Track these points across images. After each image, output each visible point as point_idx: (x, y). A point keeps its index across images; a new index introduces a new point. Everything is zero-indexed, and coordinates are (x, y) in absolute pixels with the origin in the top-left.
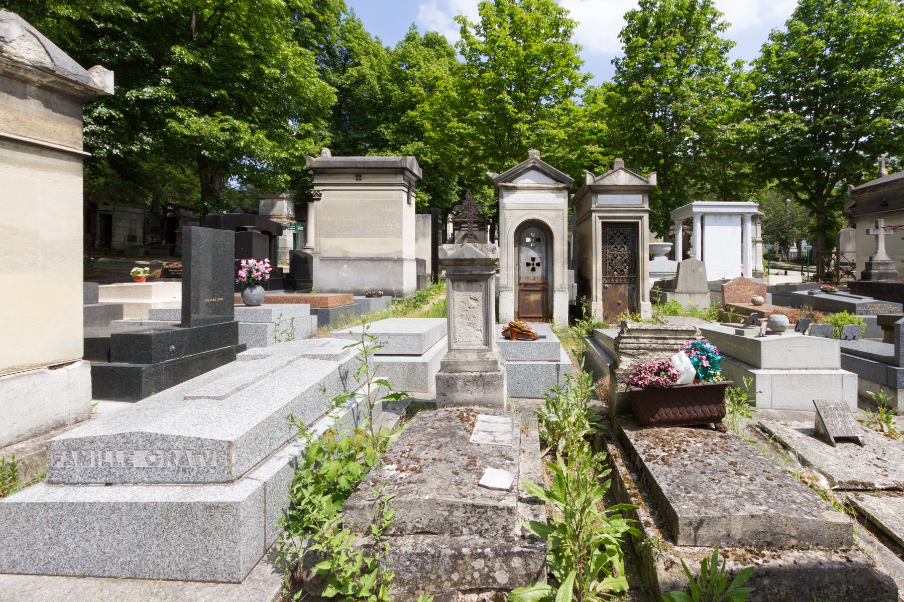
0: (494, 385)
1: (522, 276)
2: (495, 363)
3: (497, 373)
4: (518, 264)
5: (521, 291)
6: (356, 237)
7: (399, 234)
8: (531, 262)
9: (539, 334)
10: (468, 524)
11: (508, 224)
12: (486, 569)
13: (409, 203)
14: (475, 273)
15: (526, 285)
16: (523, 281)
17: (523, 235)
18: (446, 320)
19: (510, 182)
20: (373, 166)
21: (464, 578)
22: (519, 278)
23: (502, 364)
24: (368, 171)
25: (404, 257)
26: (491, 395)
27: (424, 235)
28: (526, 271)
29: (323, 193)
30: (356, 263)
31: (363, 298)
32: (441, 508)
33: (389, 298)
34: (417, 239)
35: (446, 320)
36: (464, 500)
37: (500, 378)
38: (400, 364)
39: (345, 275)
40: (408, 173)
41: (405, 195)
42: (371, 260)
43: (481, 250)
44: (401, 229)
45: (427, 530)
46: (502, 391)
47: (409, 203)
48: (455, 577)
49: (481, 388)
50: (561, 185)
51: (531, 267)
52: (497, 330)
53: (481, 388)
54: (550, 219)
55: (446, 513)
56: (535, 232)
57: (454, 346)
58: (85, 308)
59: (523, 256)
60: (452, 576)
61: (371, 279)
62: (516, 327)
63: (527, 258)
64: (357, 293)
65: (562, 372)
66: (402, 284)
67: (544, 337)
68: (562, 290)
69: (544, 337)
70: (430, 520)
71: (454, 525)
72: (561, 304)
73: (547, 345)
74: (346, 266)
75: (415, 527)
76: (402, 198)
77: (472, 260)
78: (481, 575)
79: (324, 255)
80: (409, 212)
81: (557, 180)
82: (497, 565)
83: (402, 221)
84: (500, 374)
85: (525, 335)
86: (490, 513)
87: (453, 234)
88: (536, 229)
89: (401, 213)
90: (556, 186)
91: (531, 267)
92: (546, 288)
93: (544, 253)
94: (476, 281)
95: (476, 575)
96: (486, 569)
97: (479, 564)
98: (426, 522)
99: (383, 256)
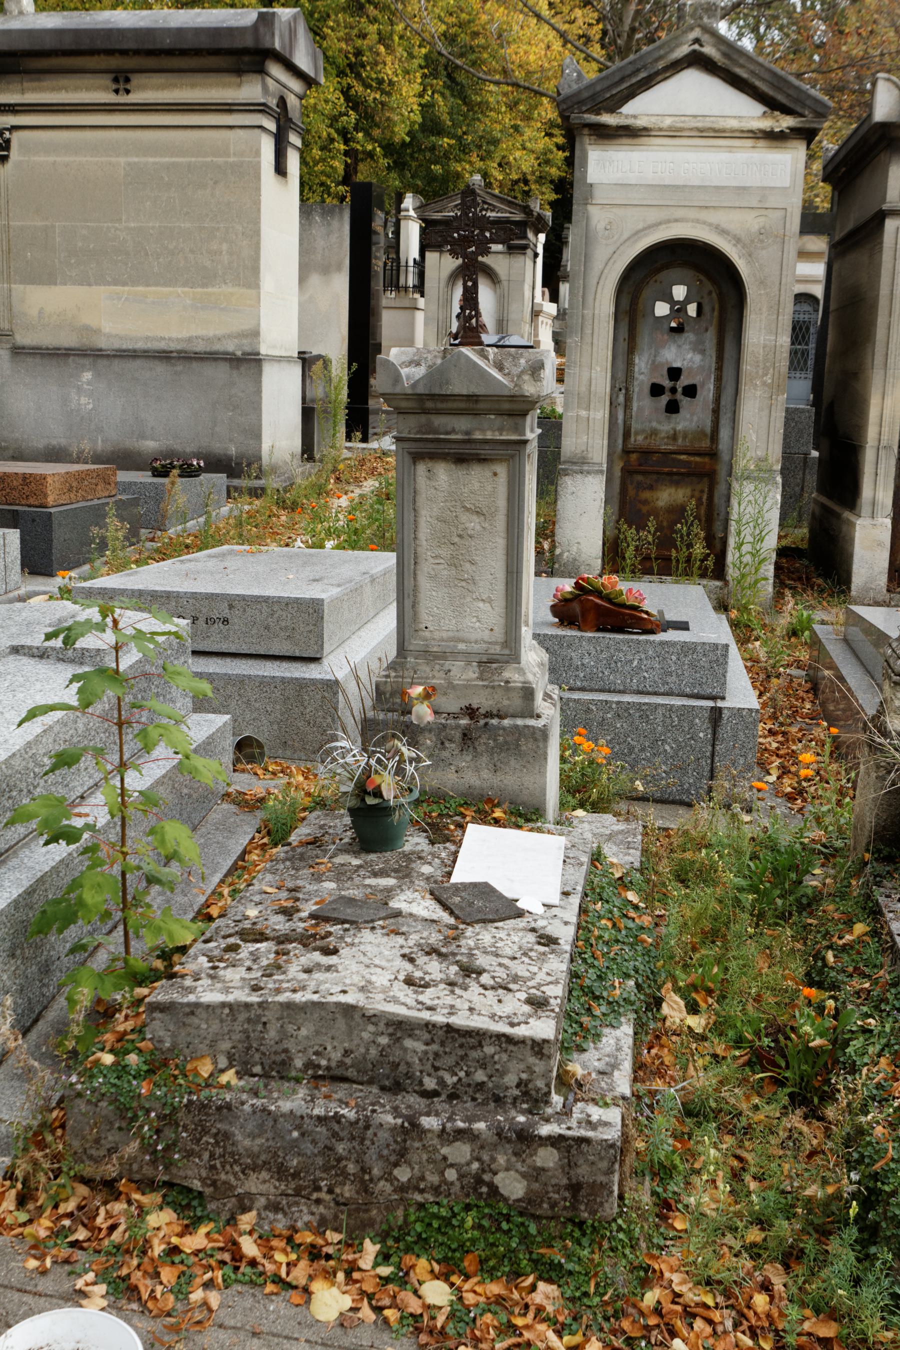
0: (520, 754)
1: (635, 426)
2: (528, 693)
3: (531, 722)
4: (622, 382)
5: (627, 472)
6: (116, 282)
7: (249, 273)
8: (667, 383)
9: (670, 616)
10: (436, 1069)
11: (600, 254)
12: (475, 1166)
13: (280, 170)
14: (478, 436)
15: (646, 453)
16: (638, 440)
17: (647, 293)
18: (389, 559)
19: (612, 110)
20: (168, 43)
21: (422, 1178)
22: (627, 434)
23: (547, 696)
24: (151, 62)
25: (264, 350)
26: (511, 779)
27: (326, 270)
28: (647, 411)
29: (16, 138)
30: (117, 365)
31: (144, 477)
32: (371, 1028)
33: (220, 479)
34: (302, 279)
35: (389, 559)
36: (426, 1015)
37: (544, 733)
38: (264, 683)
39: (86, 403)
40: (276, 70)
41: (267, 147)
42: (164, 356)
43: (500, 367)
44: (256, 259)
45: (338, 1072)
46: (542, 772)
47: (280, 170)
48: (403, 1174)
49: (485, 759)
50: (786, 122)
51: (665, 399)
52: (538, 596)
53: (485, 759)
54: (737, 240)
55: (384, 1040)
56: (692, 273)
57: (415, 644)
58: (561, 769)
59: (641, 363)
60: (396, 1172)
61: (169, 418)
62: (598, 593)
63: (654, 367)
64: (126, 459)
65: (726, 730)
66: (258, 436)
67: (683, 626)
68: (760, 475)
69: (683, 626)
70: (347, 1053)
71: (402, 1068)
72: (758, 517)
73: (687, 649)
74: (87, 376)
75: (309, 1065)
76: (258, 153)
77: (473, 398)
78: (461, 1176)
79: (23, 339)
80: (279, 203)
81: (772, 104)
82: (501, 1160)
83: (257, 233)
84: (540, 723)
85: (621, 618)
86: (489, 1050)
87: (420, 264)
88: (689, 273)
89: (257, 203)
90: (766, 124)
91: (665, 399)
92: (704, 468)
93: (712, 352)
94: (482, 460)
95: (451, 1175)
96: (475, 1166)
97: (460, 1152)
98: (336, 1056)
99: (200, 347)
